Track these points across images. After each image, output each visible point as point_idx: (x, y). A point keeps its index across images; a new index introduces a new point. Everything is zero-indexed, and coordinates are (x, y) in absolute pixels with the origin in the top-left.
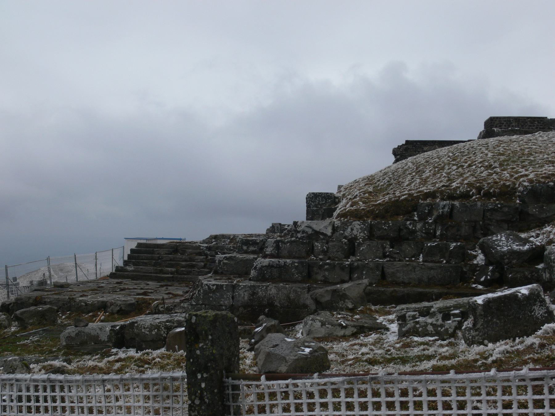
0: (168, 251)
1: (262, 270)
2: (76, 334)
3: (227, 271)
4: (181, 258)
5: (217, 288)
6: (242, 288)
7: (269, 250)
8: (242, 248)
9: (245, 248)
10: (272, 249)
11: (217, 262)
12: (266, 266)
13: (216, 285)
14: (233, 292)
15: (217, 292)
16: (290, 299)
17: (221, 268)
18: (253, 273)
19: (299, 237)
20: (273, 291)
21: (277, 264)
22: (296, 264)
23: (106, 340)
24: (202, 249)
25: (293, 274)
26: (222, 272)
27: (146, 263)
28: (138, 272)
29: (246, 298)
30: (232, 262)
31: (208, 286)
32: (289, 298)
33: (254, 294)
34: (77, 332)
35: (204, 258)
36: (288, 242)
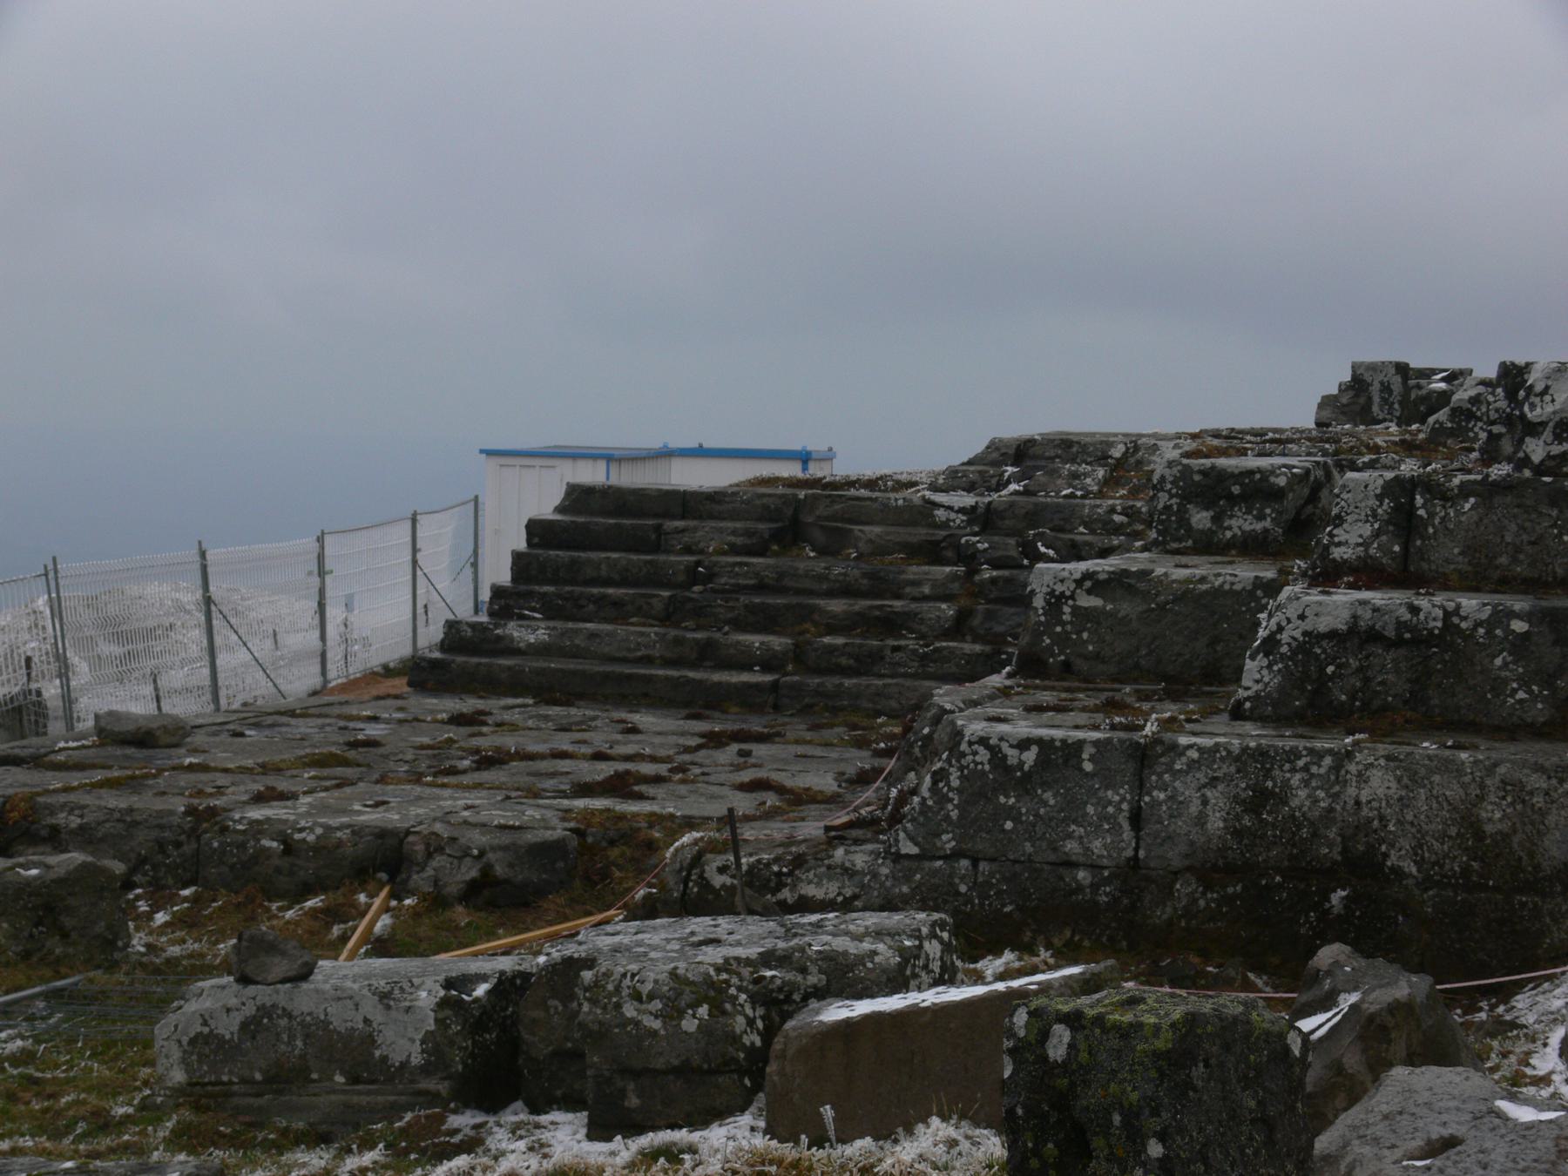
0: (748, 533)
1: (1309, 658)
2: (244, 1026)
3: (1097, 657)
4: (821, 578)
5: (1043, 762)
6: (1192, 765)
7: (1350, 538)
8: (1184, 522)
9: (1201, 518)
10: (1367, 530)
11: (1039, 602)
12: (1332, 634)
13: (1039, 741)
14: (1140, 786)
15: (1046, 785)
16: (1479, 835)
17: (1062, 640)
18: (1255, 674)
19: (1536, 458)
20: (1380, 785)
21: (1400, 625)
22: (1519, 626)
23: (417, 1059)
24: (945, 525)
25: (1498, 686)
26: (1067, 667)
27: (617, 604)
28: (576, 653)
29: (1216, 823)
30: (1128, 608)
31: (995, 751)
32: (1473, 827)
33: (1260, 800)
34: (250, 1010)
35: (954, 577)
36: (1465, 490)
